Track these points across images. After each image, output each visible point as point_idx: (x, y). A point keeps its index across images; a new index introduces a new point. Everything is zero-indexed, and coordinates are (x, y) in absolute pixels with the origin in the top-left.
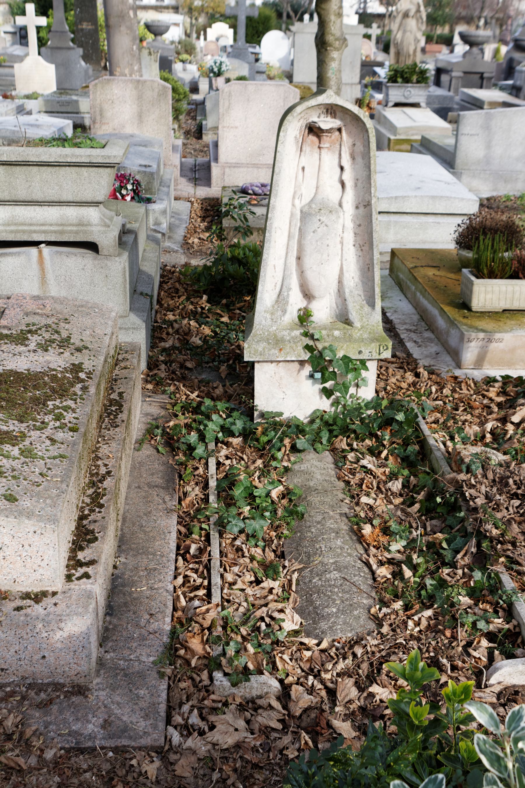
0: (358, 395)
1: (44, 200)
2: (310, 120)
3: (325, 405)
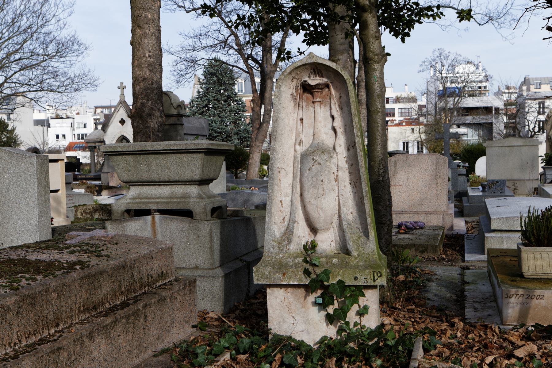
0: (362, 324)
2: (303, 80)
3: (331, 332)
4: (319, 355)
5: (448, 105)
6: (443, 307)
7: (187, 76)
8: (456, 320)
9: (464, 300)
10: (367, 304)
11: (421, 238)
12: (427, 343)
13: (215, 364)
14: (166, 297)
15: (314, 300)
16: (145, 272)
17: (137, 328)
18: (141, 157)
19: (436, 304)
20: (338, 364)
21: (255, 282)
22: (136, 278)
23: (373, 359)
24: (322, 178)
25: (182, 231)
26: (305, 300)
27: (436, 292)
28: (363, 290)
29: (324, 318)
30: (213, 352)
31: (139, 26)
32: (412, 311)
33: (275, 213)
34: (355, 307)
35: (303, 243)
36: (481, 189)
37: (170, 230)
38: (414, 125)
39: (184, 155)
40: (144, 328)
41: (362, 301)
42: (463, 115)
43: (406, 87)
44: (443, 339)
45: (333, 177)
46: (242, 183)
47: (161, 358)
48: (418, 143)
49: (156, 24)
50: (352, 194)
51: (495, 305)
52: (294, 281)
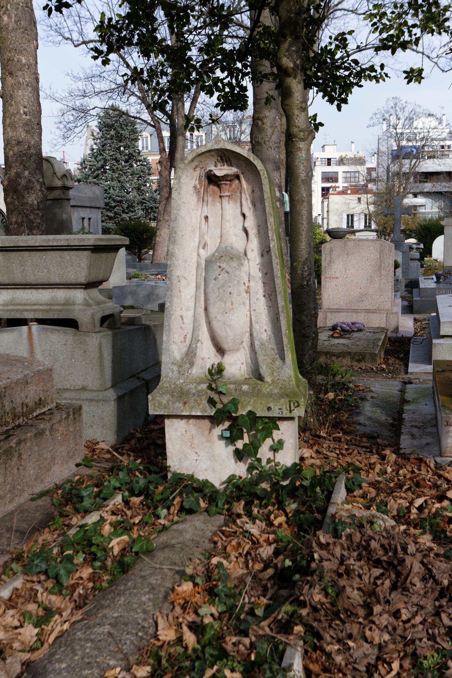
0: (277, 460)
1: (36, 283)
2: (208, 169)
3: (240, 470)
4: (225, 498)
5: (403, 169)
6: (375, 435)
7: (77, 130)
8: (387, 452)
9: (401, 424)
10: (283, 438)
11: (358, 343)
12: (350, 482)
14: (45, 429)
15: (220, 433)
16: (18, 401)
17: (9, 469)
18: (13, 254)
19: (367, 430)
21: (151, 412)
22: (7, 409)
23: (287, 503)
24: (230, 290)
25: (65, 344)
27: (369, 414)
28: (278, 422)
29: (232, 453)
30: (102, 496)
31: (11, 74)
32: (338, 440)
33: (174, 331)
35: (208, 366)
36: (435, 280)
37: (50, 346)
38: (361, 194)
39: (66, 253)
40: (18, 469)
41: (276, 435)
42: (420, 182)
43: (353, 145)
44: (370, 475)
45: (243, 288)
46: (146, 268)
47: (40, 502)
48: (366, 216)
49: (33, 71)
51: (436, 430)
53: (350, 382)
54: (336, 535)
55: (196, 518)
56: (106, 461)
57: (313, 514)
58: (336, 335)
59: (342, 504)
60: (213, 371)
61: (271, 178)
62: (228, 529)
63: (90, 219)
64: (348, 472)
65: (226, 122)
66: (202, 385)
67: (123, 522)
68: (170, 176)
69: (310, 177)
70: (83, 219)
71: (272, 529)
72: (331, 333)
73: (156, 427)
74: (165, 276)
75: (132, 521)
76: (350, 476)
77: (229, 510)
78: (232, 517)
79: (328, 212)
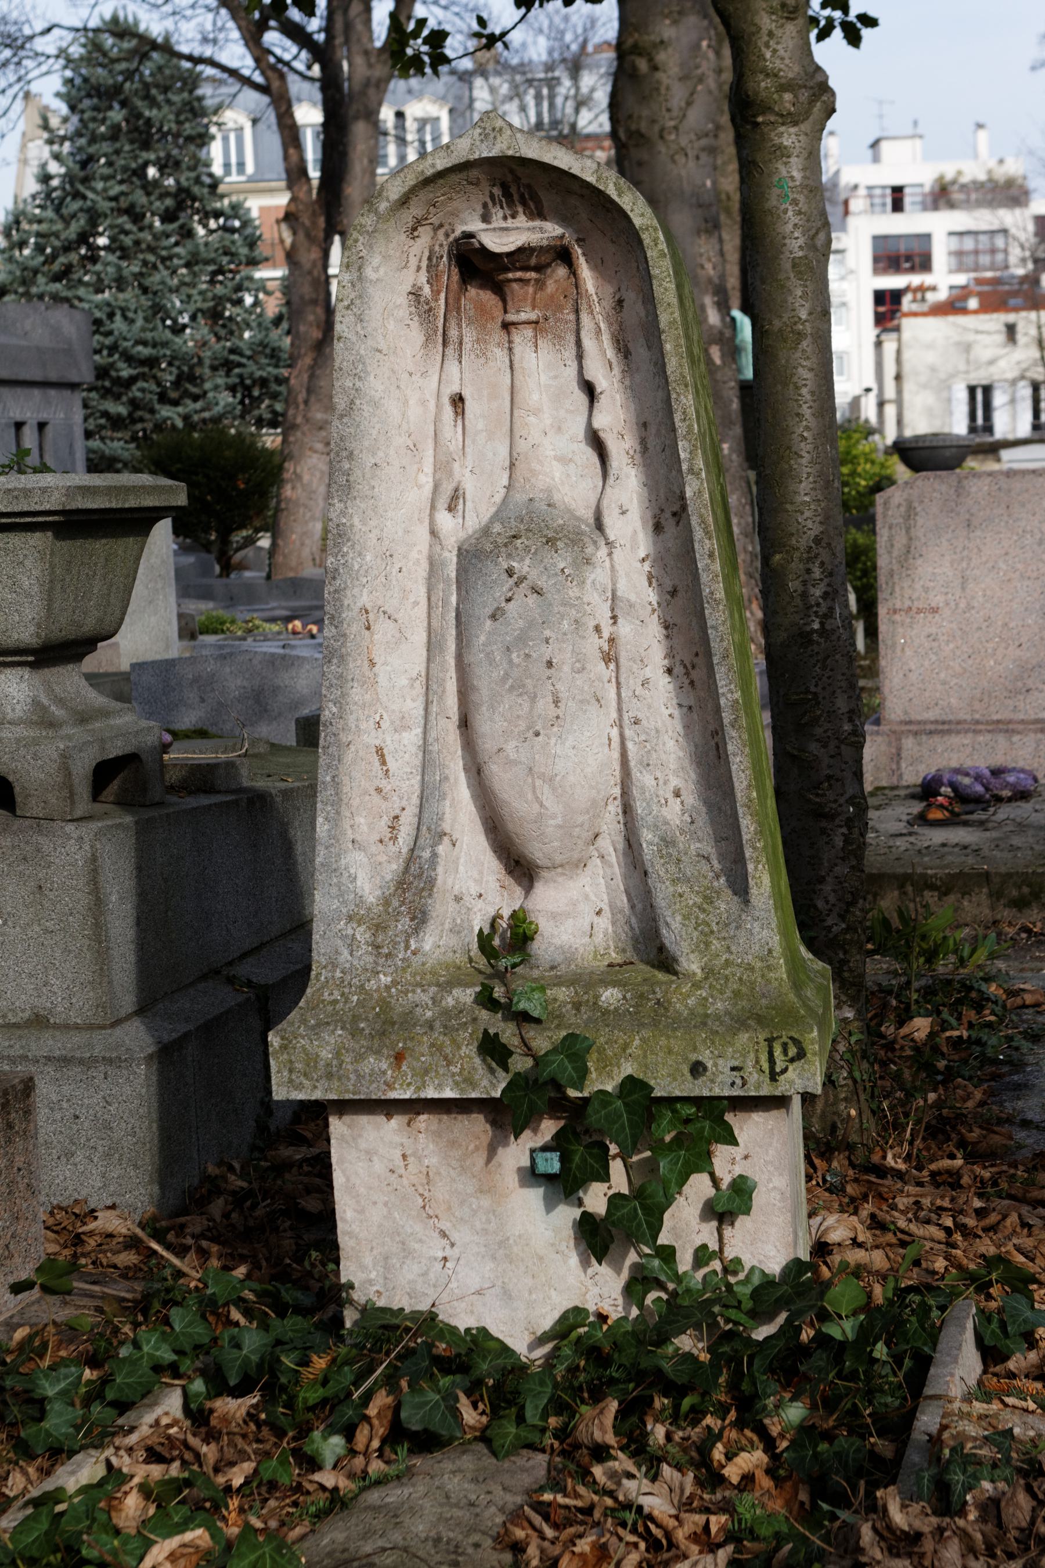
0: (729, 1253)
3: (602, 1289)
4: (549, 1390)
11: (1016, 841)
12: (995, 1325)
13: (117, 1441)
15: (526, 1162)
20: (627, 1426)
21: (280, 1093)
23: (770, 1401)
24: (547, 652)
26: (489, 1160)
28: (729, 1117)
30: (110, 1395)
32: (950, 1181)
33: (355, 802)
34: (699, 1187)
35: (479, 922)
38: (1016, 309)
41: (726, 1162)
43: (982, 135)
45: (593, 645)
46: (249, 596)
50: (676, 713)
52: (440, 1087)
53: (987, 979)
54: (945, 1501)
55: (447, 1465)
56: (124, 1276)
57: (863, 1437)
58: (936, 815)
59: (968, 1399)
60: (496, 942)
61: (686, 262)
62: (560, 1499)
63: (42, 426)
64: (983, 1288)
65: (522, 68)
66: (457, 992)
67: (188, 1483)
68: (326, 266)
69: (820, 251)
70: (19, 426)
71: (719, 1496)
72: (917, 807)
73: (298, 1154)
74: (319, 622)
75: (221, 1480)
76: (993, 1305)
77: (562, 1434)
78: (577, 1457)
79: (898, 378)
